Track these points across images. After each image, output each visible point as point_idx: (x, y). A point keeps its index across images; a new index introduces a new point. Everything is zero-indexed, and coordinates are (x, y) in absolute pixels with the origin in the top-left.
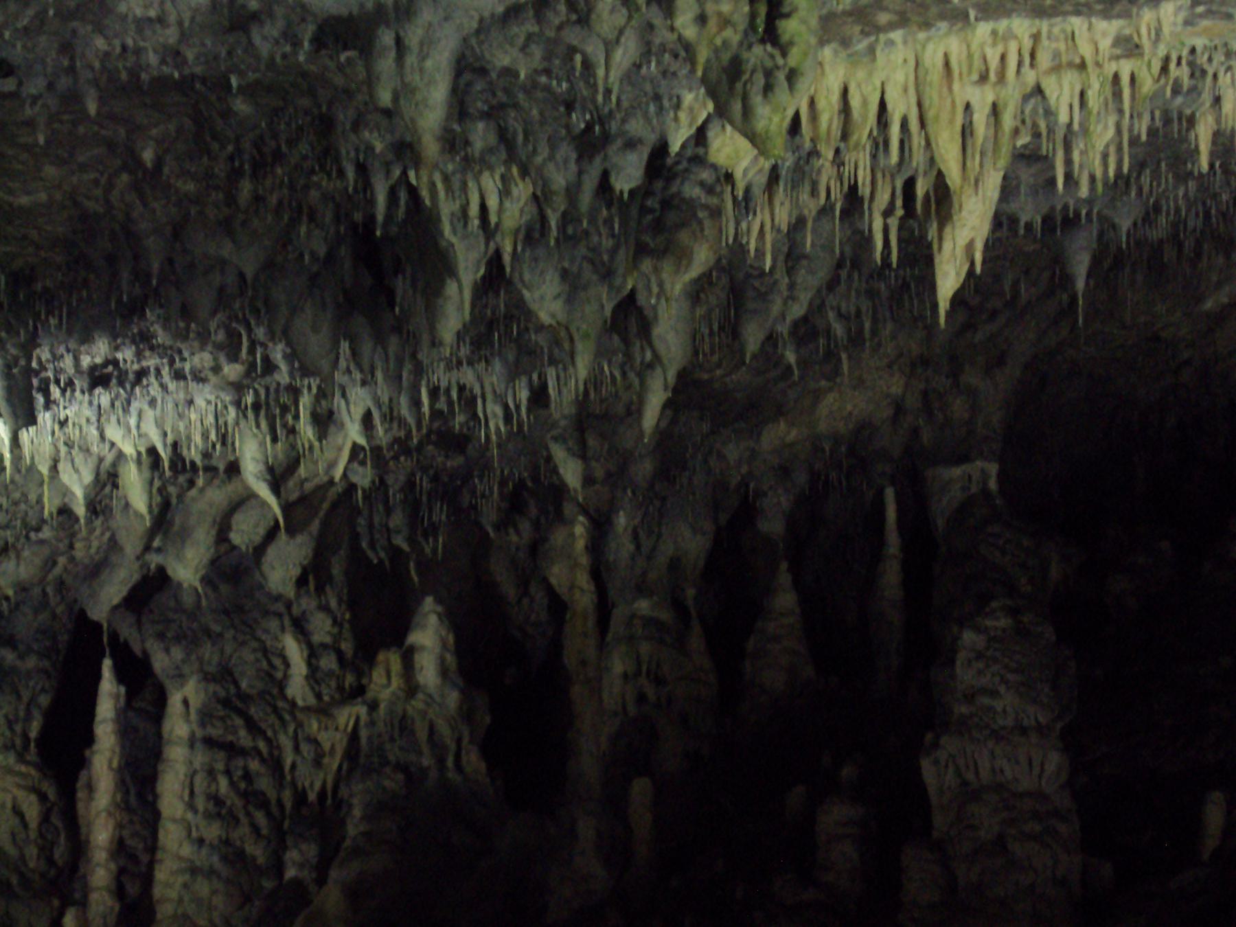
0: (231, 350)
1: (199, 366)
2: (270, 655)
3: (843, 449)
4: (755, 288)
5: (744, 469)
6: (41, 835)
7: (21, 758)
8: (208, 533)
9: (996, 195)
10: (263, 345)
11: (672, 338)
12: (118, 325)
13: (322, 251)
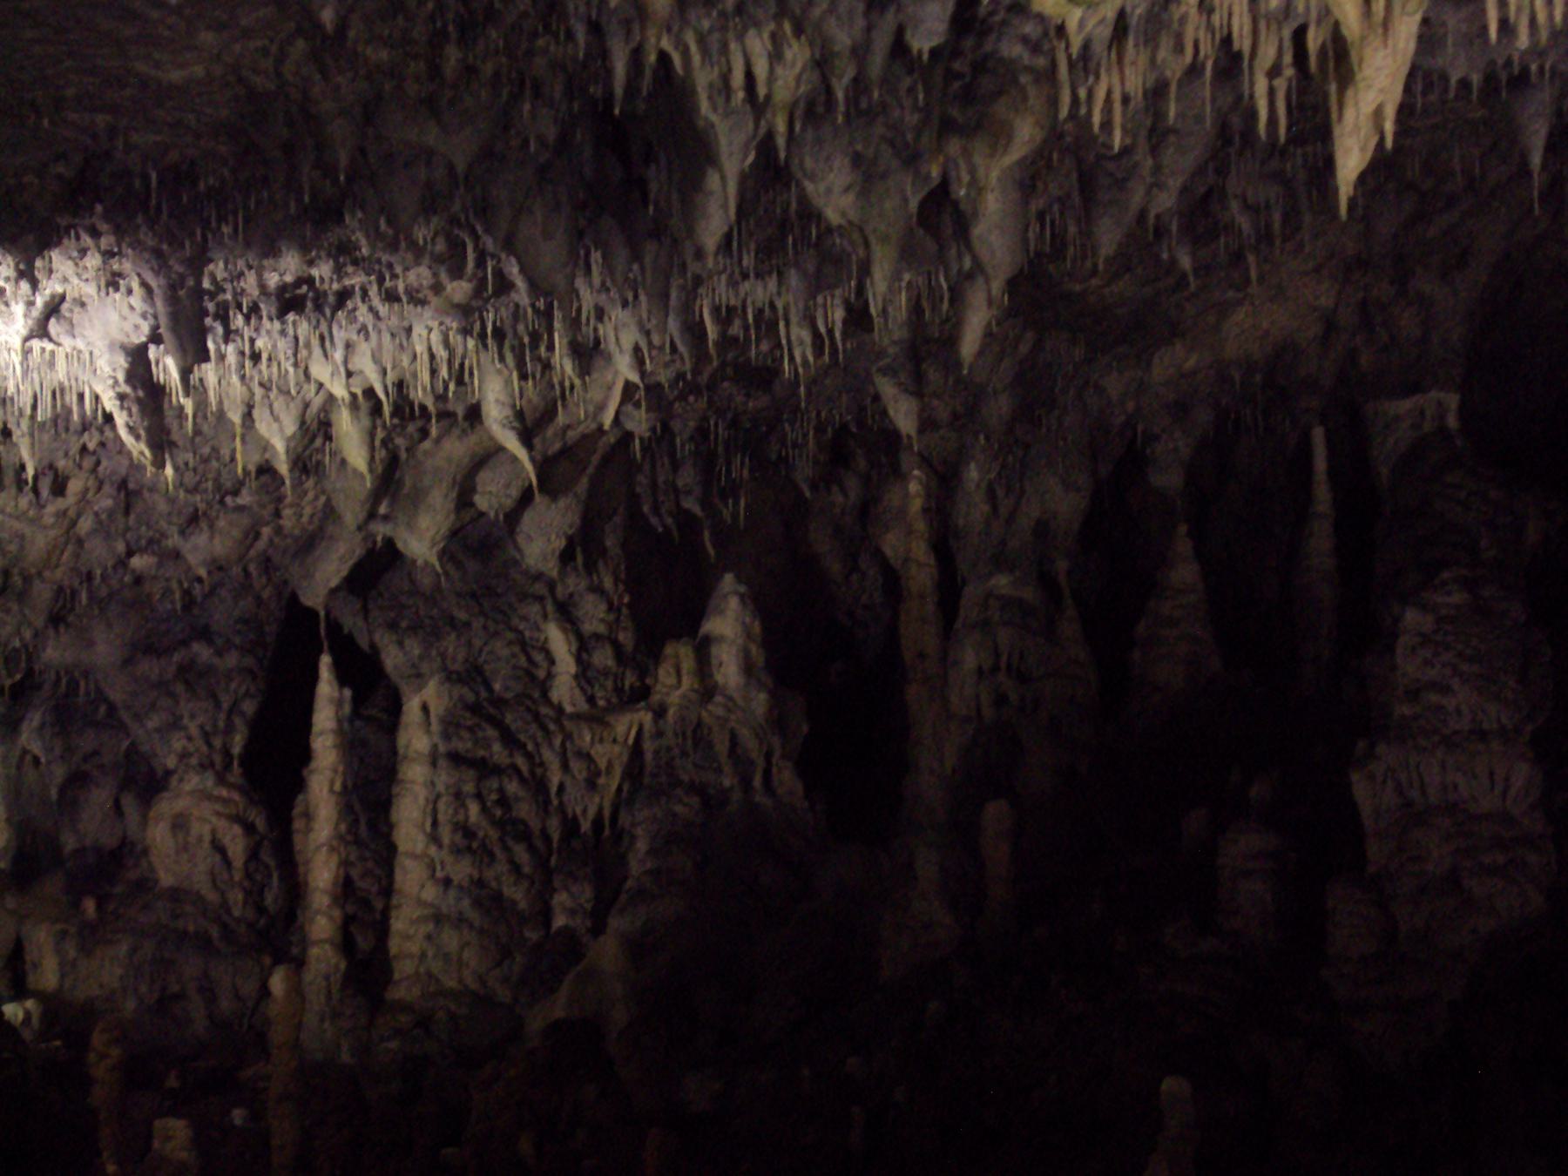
1: (415, 284)
2: (530, 649)
3: (1258, 378)
5: (1130, 405)
6: (248, 875)
7: (221, 780)
8: (446, 496)
10: (493, 256)
12: (308, 234)
13: (551, 133)
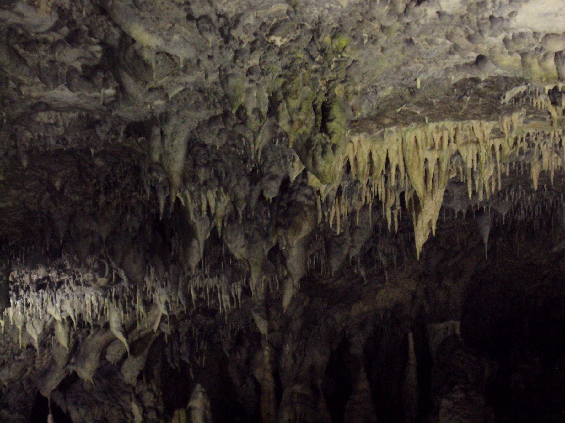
0: (101, 271)
1: (87, 279)
4: (336, 242)
5: (344, 324)
8: (96, 356)
9: (442, 200)
10: (115, 269)
11: (295, 264)
13: (137, 226)
